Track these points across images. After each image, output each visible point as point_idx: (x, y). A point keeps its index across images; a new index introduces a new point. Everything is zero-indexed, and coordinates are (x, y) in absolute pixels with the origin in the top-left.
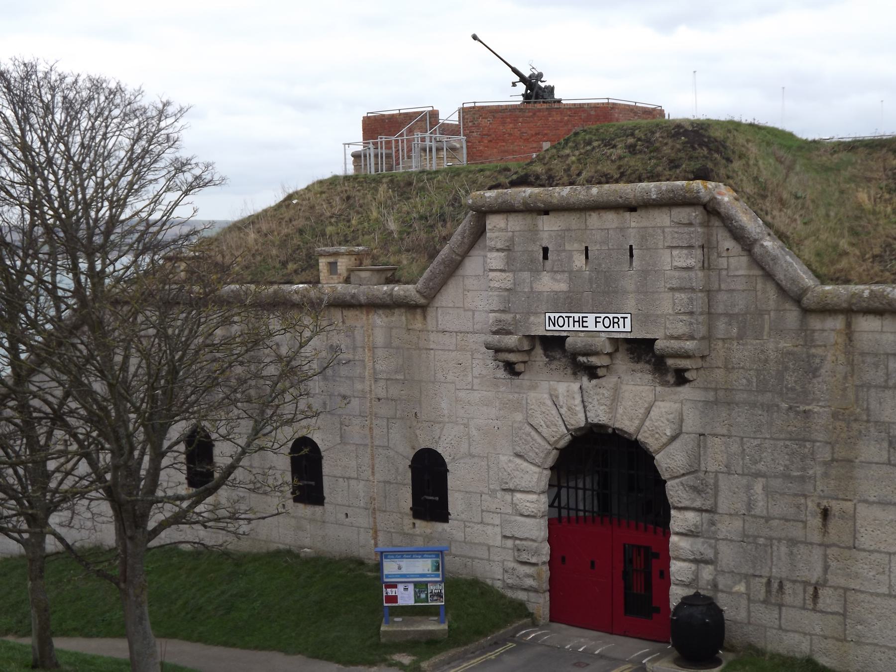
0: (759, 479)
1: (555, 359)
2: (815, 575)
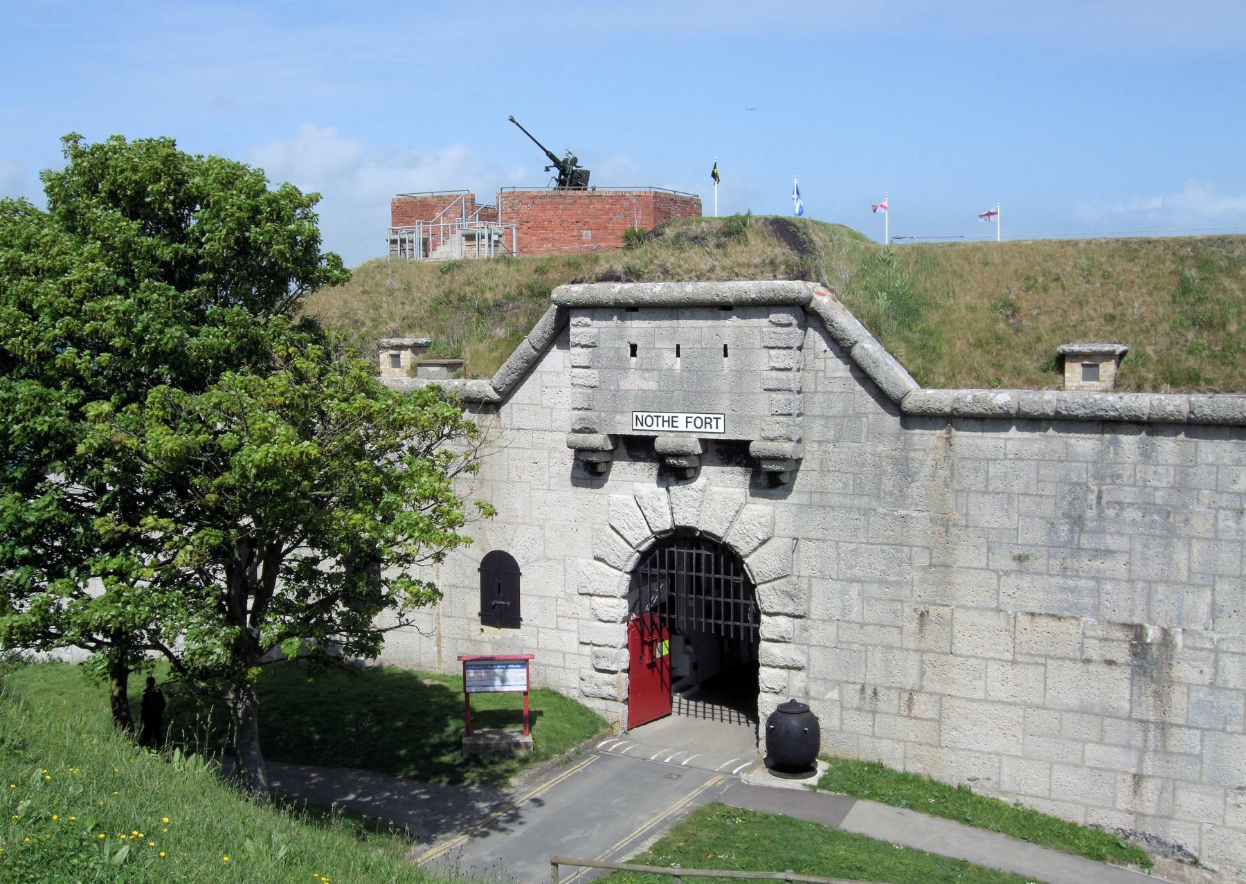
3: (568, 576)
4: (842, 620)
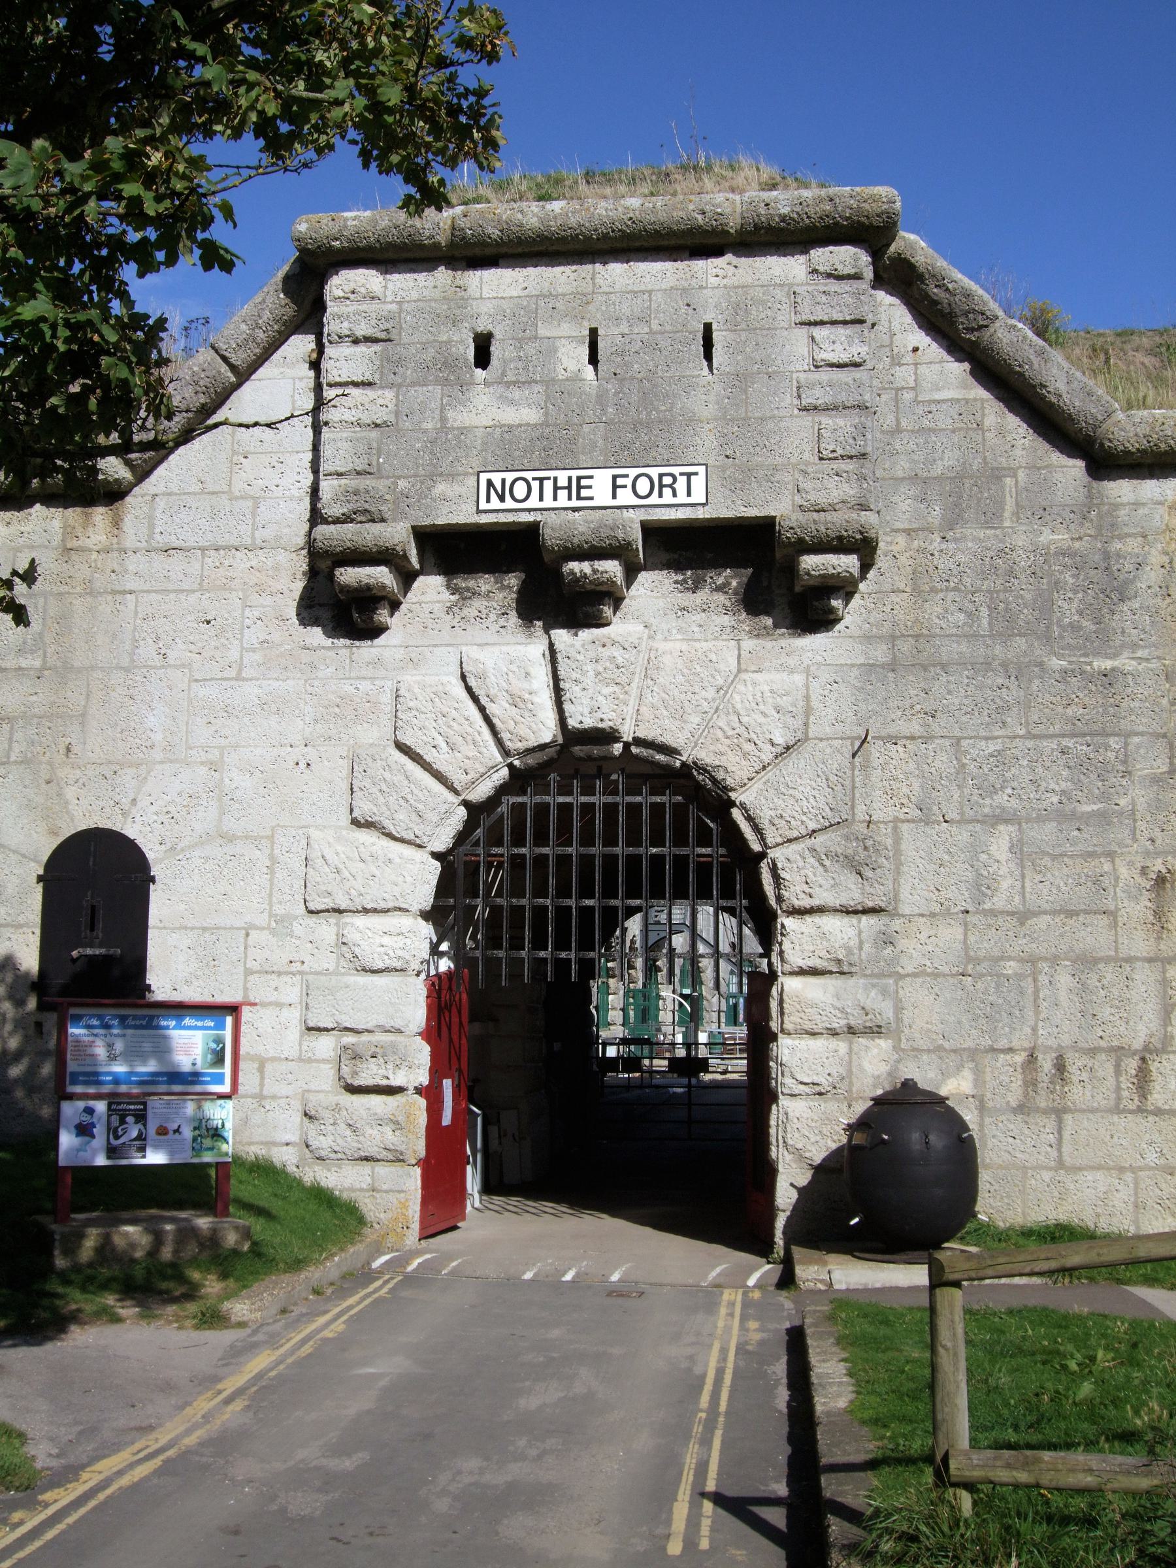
0: (1001, 828)
3: (279, 875)
4: (976, 908)
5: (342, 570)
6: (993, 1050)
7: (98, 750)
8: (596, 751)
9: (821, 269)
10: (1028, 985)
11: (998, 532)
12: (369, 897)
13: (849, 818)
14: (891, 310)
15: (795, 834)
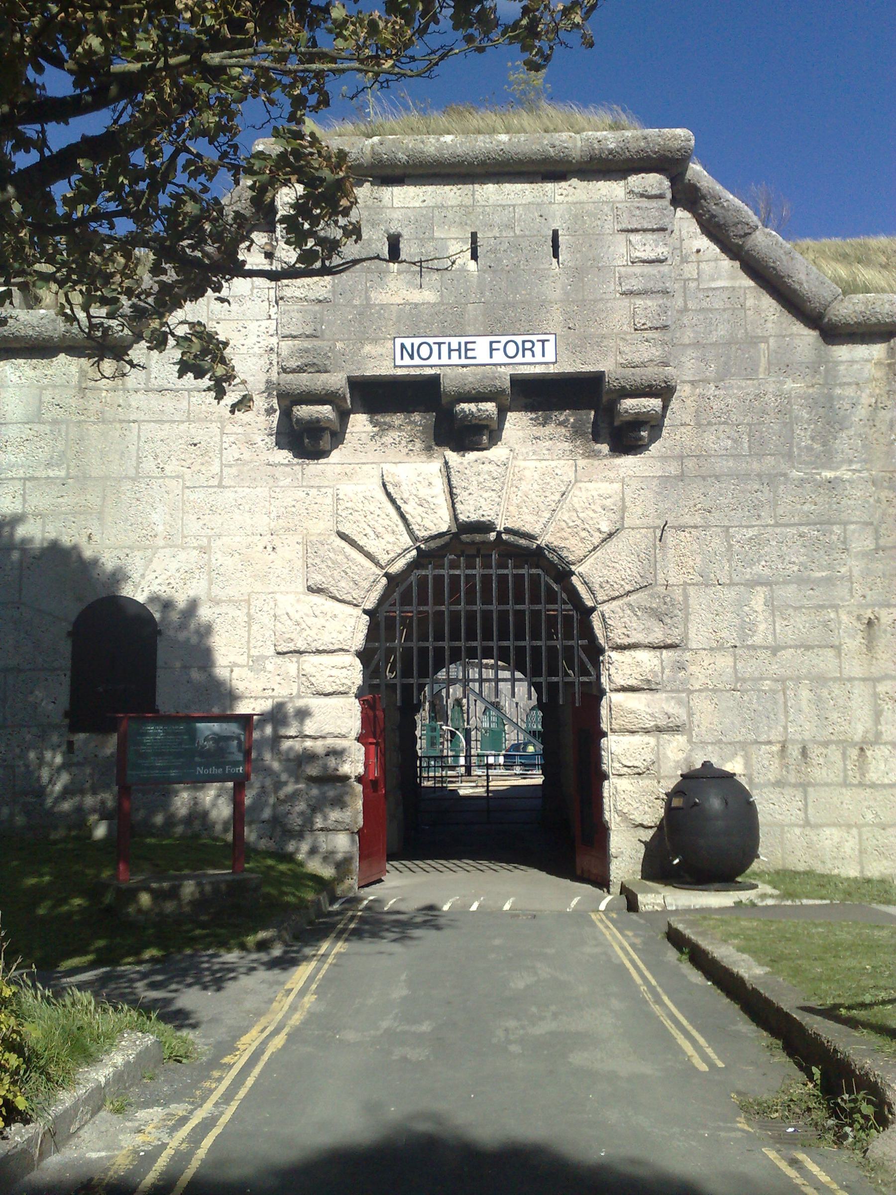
0: (758, 588)
1: (390, 427)
2: (858, 731)
3: (255, 627)
5: (299, 407)
6: (757, 742)
7: (112, 539)
8: (478, 537)
9: (636, 190)
10: (780, 697)
11: (755, 382)
12: (321, 642)
13: (653, 582)
14: (684, 222)
15: (617, 594)
